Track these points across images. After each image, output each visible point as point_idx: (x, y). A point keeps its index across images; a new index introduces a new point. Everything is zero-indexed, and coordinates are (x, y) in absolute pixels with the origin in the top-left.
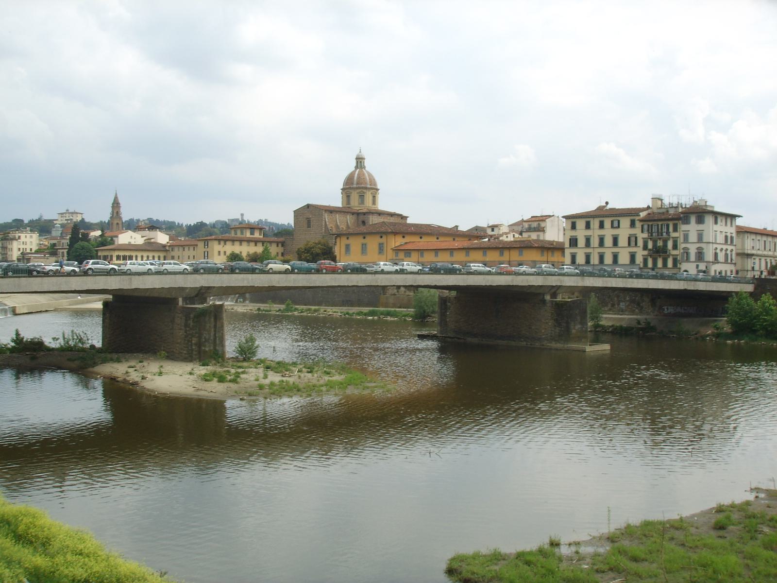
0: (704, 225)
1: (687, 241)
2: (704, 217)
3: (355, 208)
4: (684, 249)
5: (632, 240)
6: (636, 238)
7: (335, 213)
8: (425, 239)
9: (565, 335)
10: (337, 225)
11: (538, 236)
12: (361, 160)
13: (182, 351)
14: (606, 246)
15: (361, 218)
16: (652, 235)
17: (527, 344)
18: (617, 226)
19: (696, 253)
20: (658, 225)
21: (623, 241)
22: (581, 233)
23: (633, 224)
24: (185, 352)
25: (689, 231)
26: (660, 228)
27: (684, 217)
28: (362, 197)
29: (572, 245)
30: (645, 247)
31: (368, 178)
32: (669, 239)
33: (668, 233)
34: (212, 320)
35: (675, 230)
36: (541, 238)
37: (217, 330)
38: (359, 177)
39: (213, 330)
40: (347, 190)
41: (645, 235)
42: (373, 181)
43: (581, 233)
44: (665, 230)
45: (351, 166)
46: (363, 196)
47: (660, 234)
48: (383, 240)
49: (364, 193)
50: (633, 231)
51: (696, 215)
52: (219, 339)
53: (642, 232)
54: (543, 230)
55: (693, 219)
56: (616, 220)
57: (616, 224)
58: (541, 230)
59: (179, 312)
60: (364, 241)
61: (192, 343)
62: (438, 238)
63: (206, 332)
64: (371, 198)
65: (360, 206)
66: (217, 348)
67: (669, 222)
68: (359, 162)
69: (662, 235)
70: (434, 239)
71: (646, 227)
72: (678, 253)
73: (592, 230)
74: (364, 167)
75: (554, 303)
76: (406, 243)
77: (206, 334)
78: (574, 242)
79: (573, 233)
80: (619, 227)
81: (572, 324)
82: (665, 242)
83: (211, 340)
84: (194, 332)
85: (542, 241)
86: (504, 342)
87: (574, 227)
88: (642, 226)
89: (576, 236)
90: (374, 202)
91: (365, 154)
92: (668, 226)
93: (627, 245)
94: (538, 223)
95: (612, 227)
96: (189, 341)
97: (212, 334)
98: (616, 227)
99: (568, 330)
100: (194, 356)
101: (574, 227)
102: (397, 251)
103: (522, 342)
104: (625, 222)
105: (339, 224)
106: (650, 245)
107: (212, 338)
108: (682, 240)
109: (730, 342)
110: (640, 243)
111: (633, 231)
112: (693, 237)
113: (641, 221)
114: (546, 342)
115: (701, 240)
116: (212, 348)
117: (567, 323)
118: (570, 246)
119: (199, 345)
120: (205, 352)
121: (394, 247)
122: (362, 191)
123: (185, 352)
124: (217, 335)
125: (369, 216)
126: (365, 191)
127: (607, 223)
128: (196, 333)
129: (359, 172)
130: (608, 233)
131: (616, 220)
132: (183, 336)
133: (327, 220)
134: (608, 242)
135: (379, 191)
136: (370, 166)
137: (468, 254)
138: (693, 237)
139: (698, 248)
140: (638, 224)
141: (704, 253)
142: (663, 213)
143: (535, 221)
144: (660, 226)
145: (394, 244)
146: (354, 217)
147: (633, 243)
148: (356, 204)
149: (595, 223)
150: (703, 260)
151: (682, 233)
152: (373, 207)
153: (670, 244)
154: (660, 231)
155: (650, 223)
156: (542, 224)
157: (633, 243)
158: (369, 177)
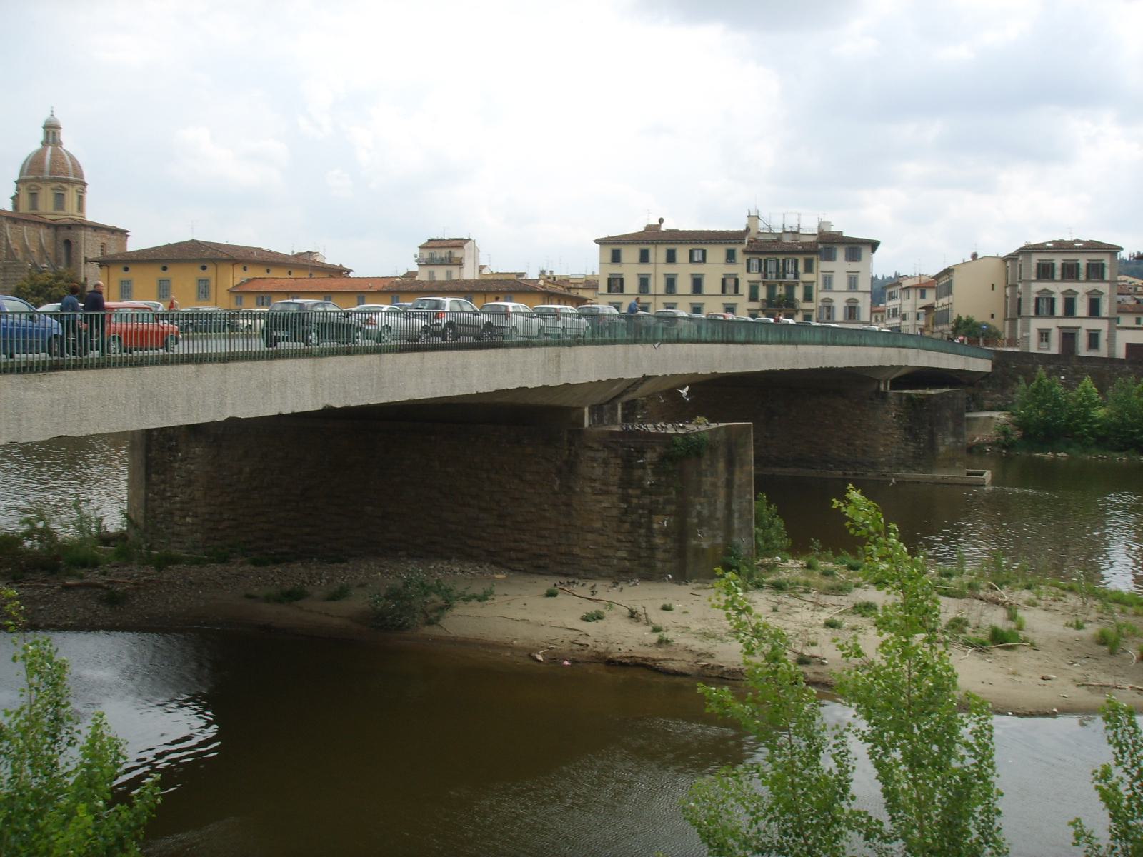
0: (860, 263)
1: (829, 288)
2: (835, 250)
3: (46, 216)
4: (824, 300)
5: (729, 285)
6: (737, 281)
7: (21, 223)
8: (275, 273)
9: (926, 456)
10: (26, 245)
11: (449, 273)
12: (54, 130)
13: (610, 552)
14: (705, 293)
15: (64, 234)
16: (765, 276)
17: (845, 474)
18: (700, 259)
19: (845, 307)
20: (778, 260)
21: (711, 284)
22: (630, 269)
23: (730, 256)
24: (621, 554)
25: (858, 272)
26: (781, 264)
27: (825, 248)
28: (60, 198)
29: (613, 288)
30: (753, 297)
31: (70, 164)
32: (797, 284)
33: (796, 275)
34: (721, 466)
35: (809, 269)
36: (455, 276)
37: (735, 492)
38: (53, 161)
39: (722, 492)
40: (34, 183)
41: (755, 276)
42: (77, 170)
43: (630, 269)
44: (790, 267)
45: (34, 142)
46: (63, 194)
47: (781, 275)
48: (210, 273)
49: (65, 189)
50: (731, 269)
51: (846, 246)
52: (741, 517)
53: (748, 271)
54: (460, 263)
55: (841, 253)
56: (698, 250)
57: (698, 256)
58: (455, 262)
59: (595, 446)
60: (163, 275)
61: (650, 529)
62: (290, 273)
63: (703, 500)
64: (76, 199)
65: (58, 212)
66: (736, 540)
67: (797, 257)
68: (51, 134)
69: (784, 277)
70: (305, 274)
71: (755, 262)
72: (812, 308)
73: (653, 265)
74: (60, 143)
75: (904, 398)
76: (249, 280)
77: (701, 504)
78: (616, 285)
79: (616, 269)
80: (704, 260)
81: (940, 436)
82: (790, 288)
83: (717, 519)
84: (661, 499)
85: (456, 282)
86: (791, 471)
87: (616, 258)
88: (748, 261)
89: (622, 274)
90: (81, 207)
91: (61, 118)
92: (796, 261)
93: (719, 291)
94: (447, 250)
95: (691, 260)
96: (636, 525)
97: (721, 503)
98: (698, 262)
99: (932, 446)
100: (659, 565)
101: (616, 258)
102: (239, 295)
103: (831, 469)
104: (716, 254)
105: (28, 244)
106: (763, 293)
107: (719, 514)
108: (820, 287)
109: (1063, 454)
110: (744, 289)
111: (731, 269)
112: (840, 282)
113: (745, 252)
114: (886, 469)
115: (855, 287)
116: (719, 540)
117: (932, 435)
118: (609, 290)
119: (681, 534)
120: (699, 552)
121: (231, 286)
122: (61, 186)
123: (621, 554)
124: (735, 507)
125: (79, 232)
126: (65, 185)
127: (682, 253)
128: (668, 502)
129: (52, 151)
130: (684, 271)
131: (698, 250)
132: (615, 512)
133: (9, 235)
134: (684, 285)
135: (88, 187)
136: (69, 142)
137: (241, 300)
138: (840, 282)
139: (848, 301)
140: (741, 258)
141: (859, 308)
142: (774, 241)
143: (442, 247)
144: (781, 262)
145: (231, 280)
146: (51, 232)
147: (730, 289)
148: (50, 208)
149: (658, 254)
150: (858, 319)
151: (820, 275)
152: (77, 216)
153: (799, 293)
154: (781, 270)
155: (763, 257)
156: (457, 254)
157: (730, 289)
158: (72, 162)
